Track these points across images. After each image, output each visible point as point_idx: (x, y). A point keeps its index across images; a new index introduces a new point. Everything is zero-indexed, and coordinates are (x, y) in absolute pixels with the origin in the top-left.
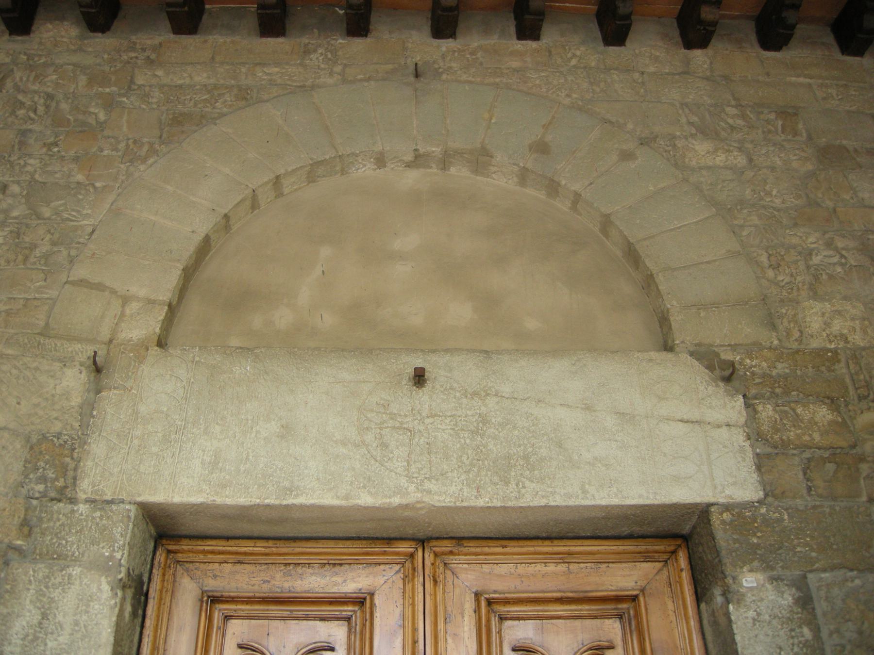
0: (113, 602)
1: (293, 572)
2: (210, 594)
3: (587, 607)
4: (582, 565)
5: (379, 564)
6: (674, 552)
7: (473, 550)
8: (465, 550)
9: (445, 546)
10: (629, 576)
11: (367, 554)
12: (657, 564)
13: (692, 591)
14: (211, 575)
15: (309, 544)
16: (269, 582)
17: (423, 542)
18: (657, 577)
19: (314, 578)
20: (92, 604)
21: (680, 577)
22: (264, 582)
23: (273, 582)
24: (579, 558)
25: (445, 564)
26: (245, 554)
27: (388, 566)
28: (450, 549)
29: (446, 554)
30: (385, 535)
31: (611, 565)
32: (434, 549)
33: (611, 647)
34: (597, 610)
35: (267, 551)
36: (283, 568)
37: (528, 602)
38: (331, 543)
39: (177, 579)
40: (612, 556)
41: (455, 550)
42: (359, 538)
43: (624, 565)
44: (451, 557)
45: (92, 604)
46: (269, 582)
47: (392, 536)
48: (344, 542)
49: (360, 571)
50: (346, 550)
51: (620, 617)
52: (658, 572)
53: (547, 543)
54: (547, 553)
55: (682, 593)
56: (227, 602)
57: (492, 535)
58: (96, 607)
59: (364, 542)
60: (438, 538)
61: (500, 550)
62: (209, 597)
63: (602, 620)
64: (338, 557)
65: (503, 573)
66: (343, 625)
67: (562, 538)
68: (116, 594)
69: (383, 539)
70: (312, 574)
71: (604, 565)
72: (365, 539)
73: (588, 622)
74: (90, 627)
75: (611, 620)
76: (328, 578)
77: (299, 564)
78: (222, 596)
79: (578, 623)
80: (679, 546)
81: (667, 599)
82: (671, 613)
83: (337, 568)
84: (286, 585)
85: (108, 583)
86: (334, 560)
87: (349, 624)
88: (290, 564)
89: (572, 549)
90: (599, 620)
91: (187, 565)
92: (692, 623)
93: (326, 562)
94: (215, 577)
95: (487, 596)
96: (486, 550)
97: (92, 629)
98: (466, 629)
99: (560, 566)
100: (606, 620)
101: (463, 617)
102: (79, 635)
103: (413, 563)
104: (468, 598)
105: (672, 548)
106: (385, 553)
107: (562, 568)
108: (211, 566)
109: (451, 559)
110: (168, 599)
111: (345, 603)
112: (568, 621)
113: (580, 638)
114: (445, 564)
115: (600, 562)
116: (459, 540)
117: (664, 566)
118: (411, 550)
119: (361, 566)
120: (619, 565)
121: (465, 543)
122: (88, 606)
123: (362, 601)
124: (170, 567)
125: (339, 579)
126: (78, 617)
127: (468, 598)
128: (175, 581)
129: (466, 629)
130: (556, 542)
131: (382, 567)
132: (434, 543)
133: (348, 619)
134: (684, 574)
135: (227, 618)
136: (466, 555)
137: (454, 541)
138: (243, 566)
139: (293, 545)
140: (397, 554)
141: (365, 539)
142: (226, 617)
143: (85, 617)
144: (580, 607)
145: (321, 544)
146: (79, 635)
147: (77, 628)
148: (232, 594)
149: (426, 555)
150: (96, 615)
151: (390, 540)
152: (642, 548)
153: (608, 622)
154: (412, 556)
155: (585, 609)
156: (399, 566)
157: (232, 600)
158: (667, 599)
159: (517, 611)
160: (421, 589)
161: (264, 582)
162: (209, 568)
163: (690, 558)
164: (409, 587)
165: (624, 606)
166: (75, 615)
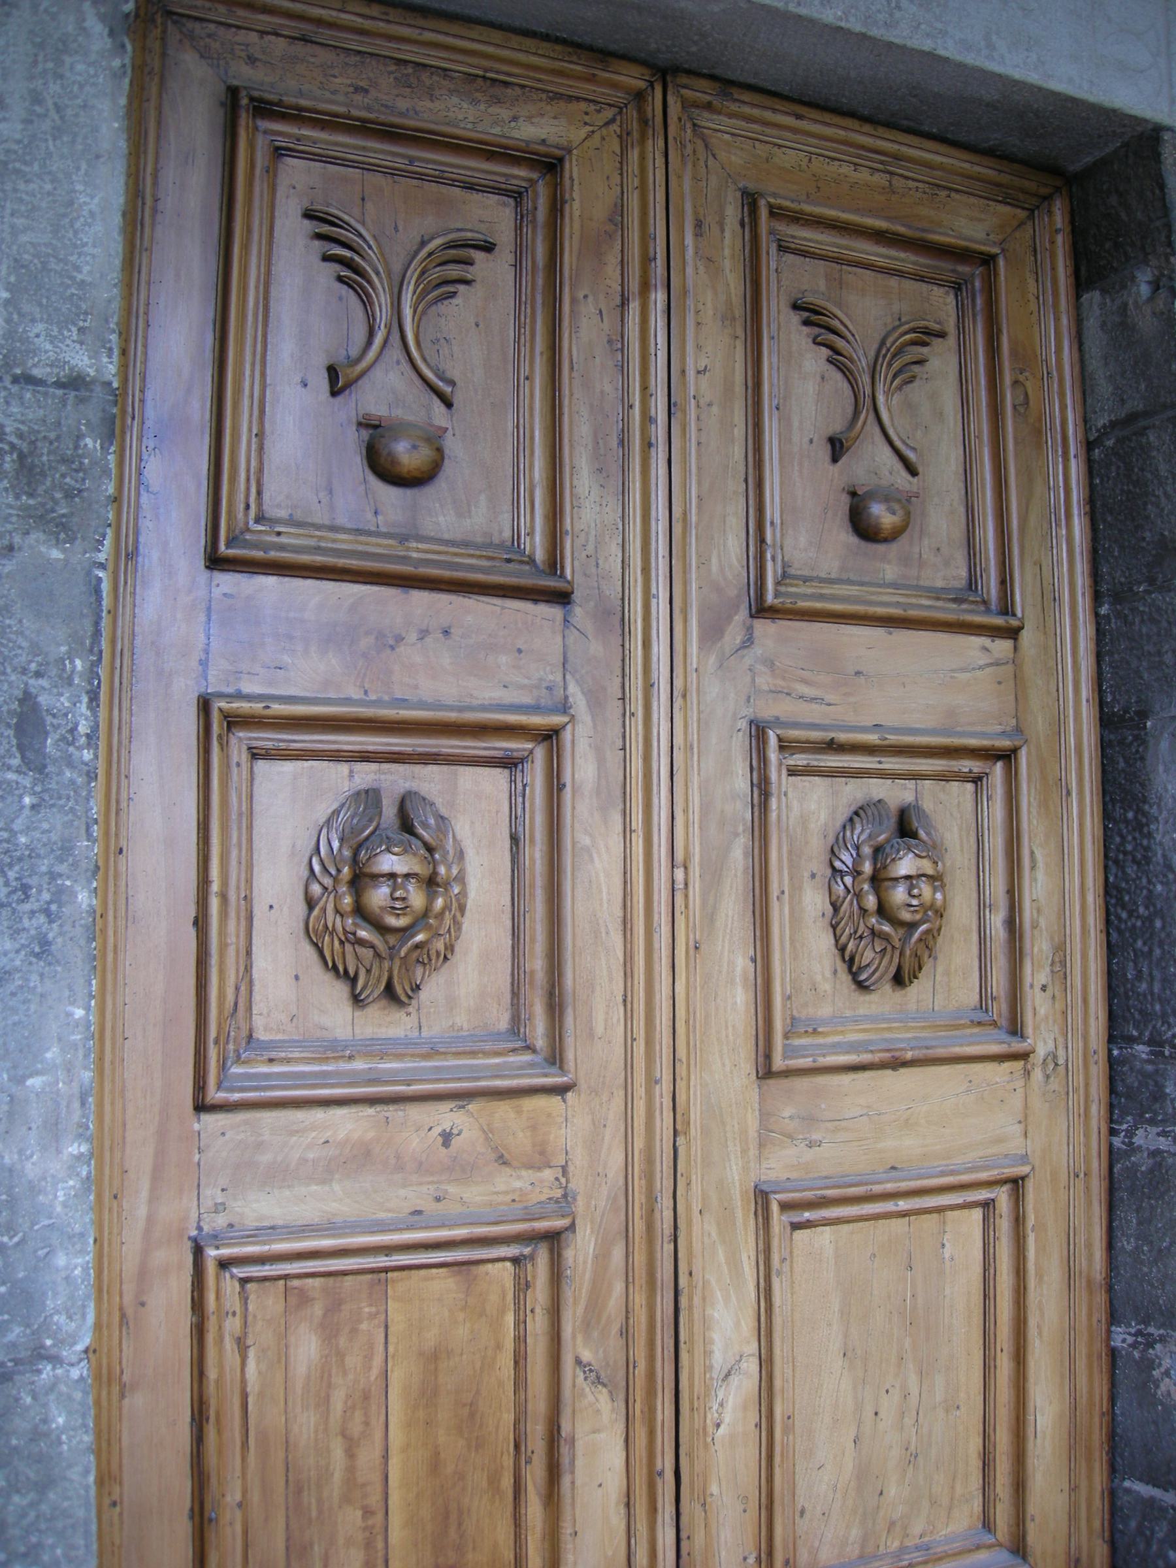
0: (117, 63)
1: (413, 80)
2: (256, 94)
3: (913, 258)
4: (911, 184)
5: (578, 99)
6: (1047, 198)
7: (747, 110)
8: (734, 107)
9: (701, 91)
10: (980, 220)
11: (560, 73)
12: (1019, 211)
13: (1070, 270)
14: (243, 54)
15: (455, 28)
16: (366, 91)
17: (665, 73)
18: (1017, 234)
19: (455, 100)
20: (68, 60)
21: (1053, 242)
22: (358, 89)
23: (373, 93)
24: (908, 169)
25: (694, 125)
26: (319, 22)
27: (593, 107)
28: (708, 98)
29: (697, 107)
30: (600, 43)
31: (953, 194)
32: (684, 91)
33: (942, 335)
34: (928, 266)
35: (368, 24)
36: (393, 68)
37: (834, 227)
38: (497, 36)
39: (170, 52)
40: (959, 179)
41: (716, 103)
42: (546, 38)
43: (972, 200)
44: (706, 114)
45: (68, 60)
46: (366, 91)
47: (613, 47)
48: (520, 39)
49: (543, 104)
50: (521, 57)
51: (957, 288)
52: (1019, 226)
53: (867, 128)
54: (863, 147)
55: (1053, 269)
56: (283, 117)
57: (785, 89)
58: (80, 67)
59: (558, 48)
60: (689, 72)
61: (789, 121)
62: (252, 99)
63: (930, 287)
64: (505, 68)
65: (788, 166)
66: (504, 204)
67: (888, 125)
68: (123, 46)
69: (591, 49)
70: (451, 92)
71: (944, 193)
72: (564, 42)
73: (908, 285)
74: (69, 112)
75: (942, 290)
76: (482, 107)
77: (425, 66)
78: (280, 103)
79: (894, 282)
80: (1058, 189)
81: (1028, 274)
82: (1032, 299)
83: (498, 91)
84: (402, 104)
85: (102, 18)
86: (497, 72)
87: (518, 203)
88: (406, 62)
89: (904, 149)
90: (924, 285)
91: (190, 25)
92: (1064, 321)
93: (481, 73)
94: (252, 60)
95: (772, 200)
96: (768, 115)
97: (76, 115)
98: (727, 252)
99: (877, 176)
100: (935, 288)
101: (723, 231)
102: (46, 125)
103: (641, 111)
104: (730, 199)
105: (1044, 191)
106: (591, 79)
107: (880, 179)
108: (242, 36)
109: (707, 120)
110: (154, 90)
111: (516, 161)
112: (879, 276)
113: (896, 308)
114: (694, 125)
115: (938, 186)
116: (727, 85)
117: (1028, 218)
118: (642, 84)
119: (544, 96)
120: (964, 198)
121: (736, 93)
122: (59, 62)
123: (550, 165)
124: (153, 21)
125: (505, 113)
126: (38, 84)
127: (730, 199)
128: (164, 55)
129: (727, 252)
130: (881, 131)
131: (583, 106)
132: (684, 80)
133: (517, 196)
134: (1059, 239)
135: (278, 153)
136: (731, 115)
137: (717, 85)
138: (310, 48)
139: (421, 22)
140: (614, 85)
141: (564, 42)
142: (277, 149)
143: (55, 87)
144: (902, 255)
145: (476, 32)
146: (46, 125)
147: (38, 109)
148: (303, 102)
149: (671, 99)
150: (81, 87)
151: (604, 55)
152: (1005, 178)
153: (937, 291)
154: (639, 96)
155: (906, 259)
156: (615, 110)
157: (297, 116)
158: (1028, 274)
159: (805, 239)
160: (660, 161)
161: (358, 89)
162: (238, 39)
163: (1072, 213)
164: (634, 155)
165: (964, 269)
166: (31, 78)
